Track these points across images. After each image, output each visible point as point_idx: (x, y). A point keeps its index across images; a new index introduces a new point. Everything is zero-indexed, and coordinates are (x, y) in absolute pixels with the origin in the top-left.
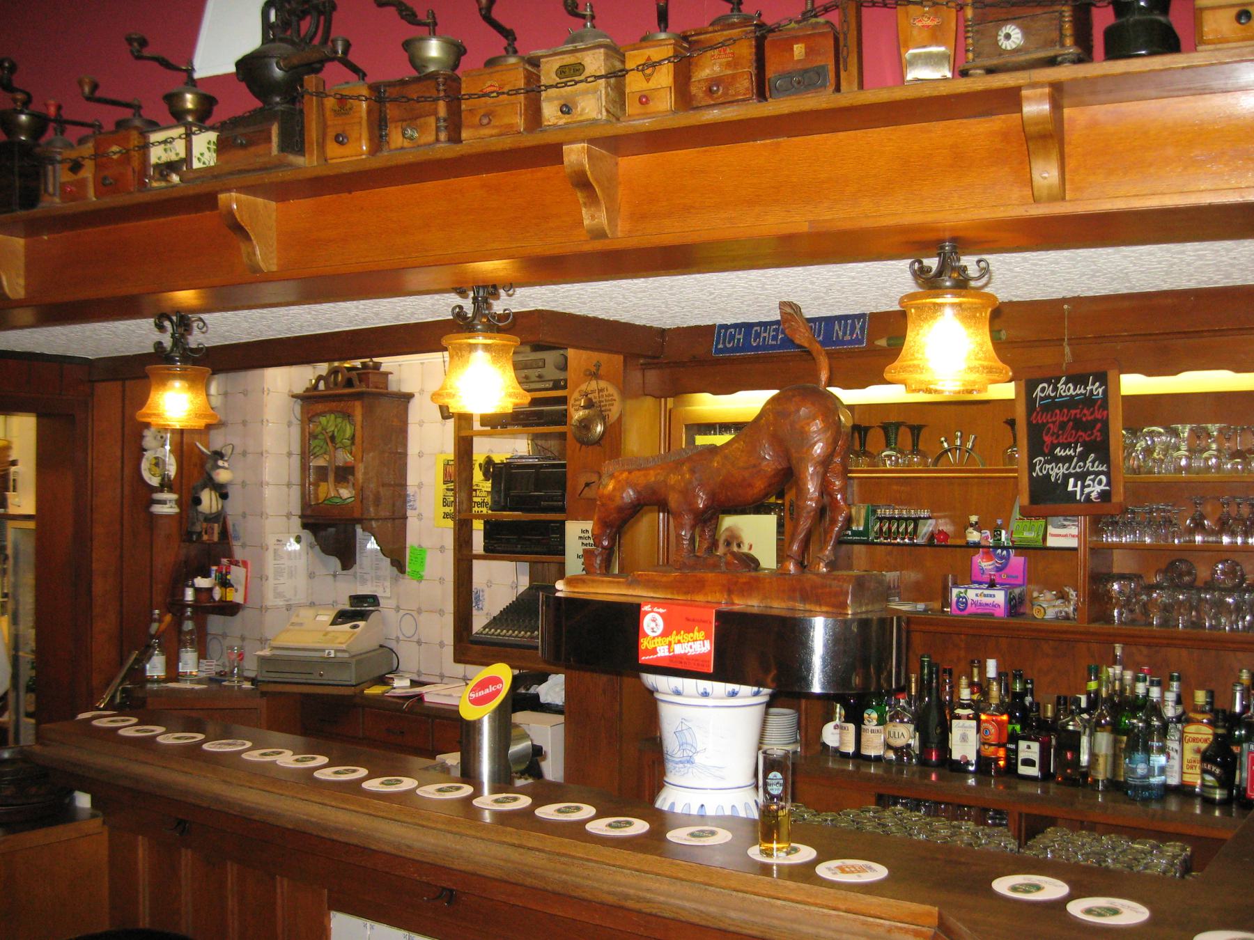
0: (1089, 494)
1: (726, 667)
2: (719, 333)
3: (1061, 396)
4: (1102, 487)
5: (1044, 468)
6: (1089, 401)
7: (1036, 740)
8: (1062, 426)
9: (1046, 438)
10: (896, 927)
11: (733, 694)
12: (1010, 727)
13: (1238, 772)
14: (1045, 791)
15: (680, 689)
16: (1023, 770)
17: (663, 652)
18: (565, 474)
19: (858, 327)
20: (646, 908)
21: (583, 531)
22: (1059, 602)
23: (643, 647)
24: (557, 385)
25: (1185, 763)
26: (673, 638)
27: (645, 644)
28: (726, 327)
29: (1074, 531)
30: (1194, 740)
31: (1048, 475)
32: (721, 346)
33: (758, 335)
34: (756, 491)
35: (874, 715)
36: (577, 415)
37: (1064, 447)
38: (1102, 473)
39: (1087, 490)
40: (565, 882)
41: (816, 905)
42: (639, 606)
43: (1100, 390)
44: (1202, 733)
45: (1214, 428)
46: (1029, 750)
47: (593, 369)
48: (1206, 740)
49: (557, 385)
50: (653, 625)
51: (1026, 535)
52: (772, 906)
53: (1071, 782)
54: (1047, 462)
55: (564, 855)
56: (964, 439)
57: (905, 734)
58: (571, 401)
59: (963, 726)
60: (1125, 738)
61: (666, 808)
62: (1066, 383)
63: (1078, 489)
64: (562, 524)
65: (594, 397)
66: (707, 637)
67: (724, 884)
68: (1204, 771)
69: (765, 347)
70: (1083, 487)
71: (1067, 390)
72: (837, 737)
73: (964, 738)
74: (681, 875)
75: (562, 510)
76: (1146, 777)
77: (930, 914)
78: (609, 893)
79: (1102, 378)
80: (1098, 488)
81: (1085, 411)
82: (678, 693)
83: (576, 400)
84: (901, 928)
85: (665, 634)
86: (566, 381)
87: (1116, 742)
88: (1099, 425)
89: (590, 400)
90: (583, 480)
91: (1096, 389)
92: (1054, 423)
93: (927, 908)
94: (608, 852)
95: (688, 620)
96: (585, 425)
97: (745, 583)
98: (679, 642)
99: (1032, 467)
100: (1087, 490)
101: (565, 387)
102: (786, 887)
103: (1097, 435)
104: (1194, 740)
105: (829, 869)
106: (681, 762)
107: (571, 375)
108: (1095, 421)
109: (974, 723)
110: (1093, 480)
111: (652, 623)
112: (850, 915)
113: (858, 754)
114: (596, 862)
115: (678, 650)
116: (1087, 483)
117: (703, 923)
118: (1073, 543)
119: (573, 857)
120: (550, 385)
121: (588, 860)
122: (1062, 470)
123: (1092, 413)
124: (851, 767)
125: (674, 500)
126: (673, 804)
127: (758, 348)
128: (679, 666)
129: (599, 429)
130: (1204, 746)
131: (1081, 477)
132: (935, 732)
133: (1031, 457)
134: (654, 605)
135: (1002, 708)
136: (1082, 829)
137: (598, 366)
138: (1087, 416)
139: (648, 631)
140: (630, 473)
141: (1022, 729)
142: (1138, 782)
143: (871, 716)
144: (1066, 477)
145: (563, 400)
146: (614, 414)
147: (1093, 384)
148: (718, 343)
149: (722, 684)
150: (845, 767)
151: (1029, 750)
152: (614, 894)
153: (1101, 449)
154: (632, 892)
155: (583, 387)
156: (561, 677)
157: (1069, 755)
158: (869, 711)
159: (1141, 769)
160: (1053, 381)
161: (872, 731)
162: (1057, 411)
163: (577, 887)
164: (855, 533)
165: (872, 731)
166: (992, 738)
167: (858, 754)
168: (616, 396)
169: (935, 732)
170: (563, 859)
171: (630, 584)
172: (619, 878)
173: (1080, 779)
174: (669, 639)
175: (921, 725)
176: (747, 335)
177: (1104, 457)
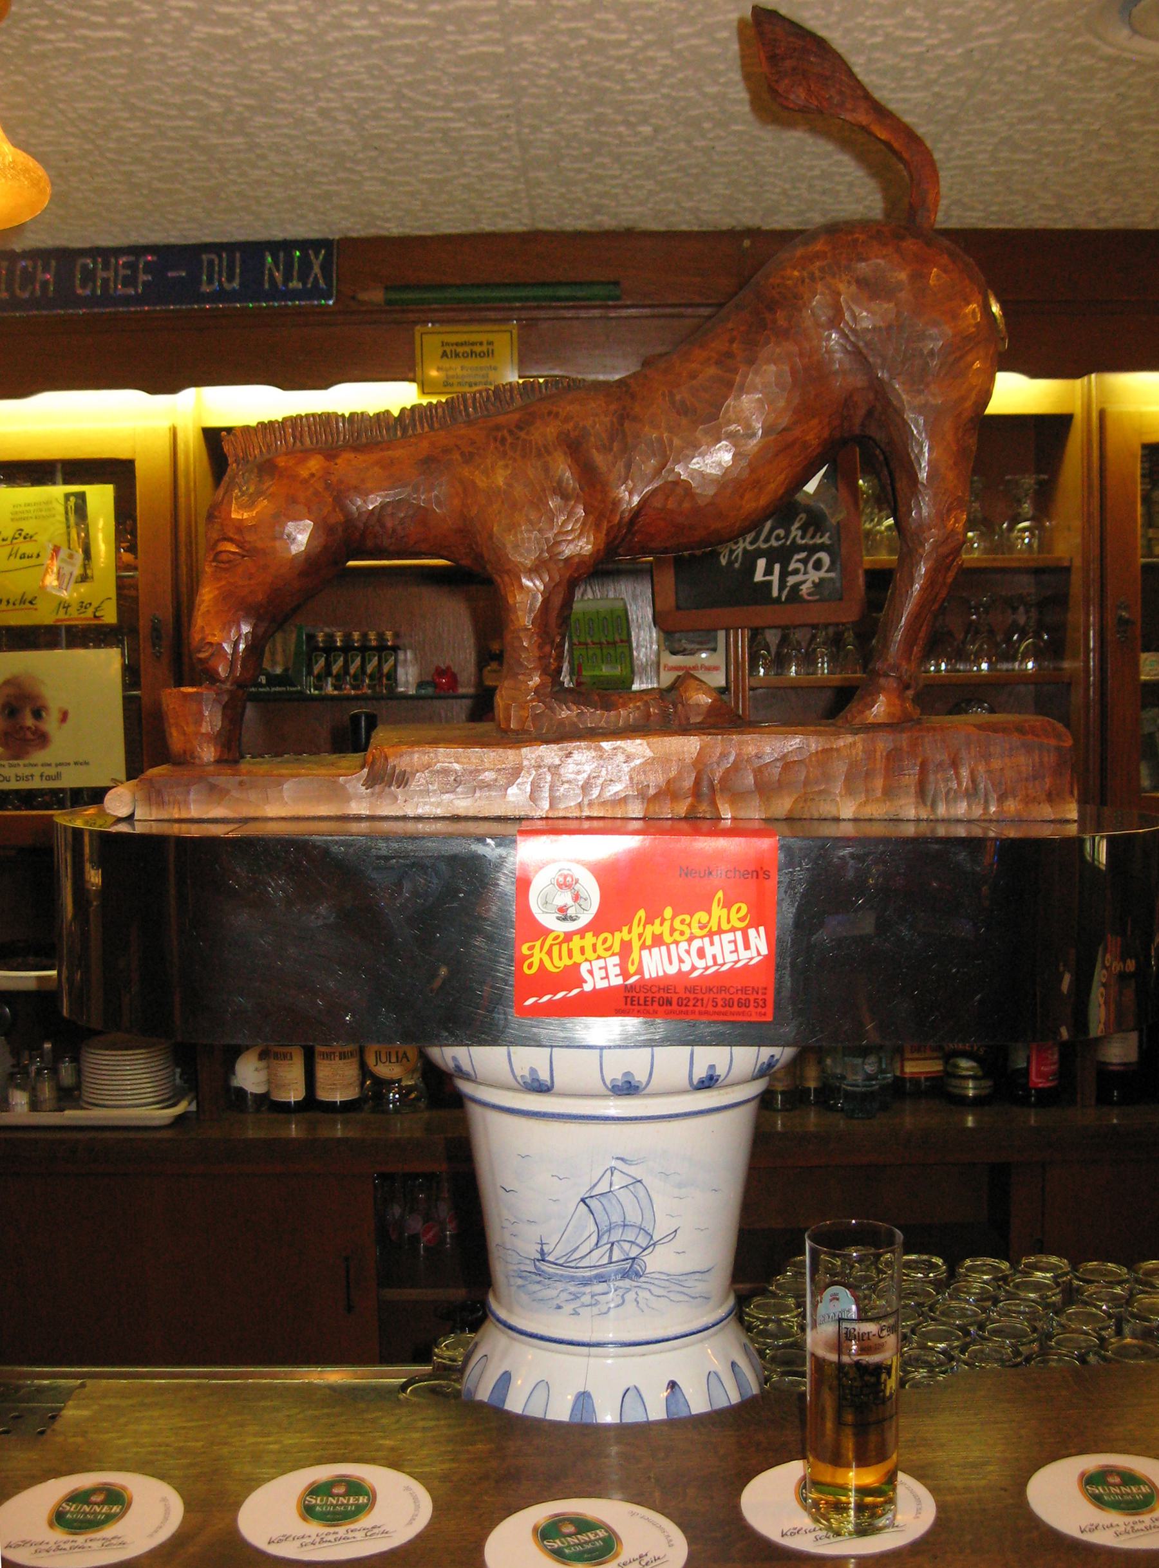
0: (796, 587)
4: (822, 574)
19: (317, 269)
26: (636, 931)
33: (89, 276)
38: (822, 548)
39: (792, 580)
63: (775, 578)
69: (107, 299)
72: (262, 1076)
80: (814, 576)
82: (541, 1088)
98: (658, 941)
100: (792, 580)
110: (805, 562)
113: (310, 1103)
116: (792, 566)
127: (93, 301)
131: (780, 556)
139: (548, 920)
150: (282, 1134)
164: (273, 680)
167: (310, 1103)
174: (624, 934)
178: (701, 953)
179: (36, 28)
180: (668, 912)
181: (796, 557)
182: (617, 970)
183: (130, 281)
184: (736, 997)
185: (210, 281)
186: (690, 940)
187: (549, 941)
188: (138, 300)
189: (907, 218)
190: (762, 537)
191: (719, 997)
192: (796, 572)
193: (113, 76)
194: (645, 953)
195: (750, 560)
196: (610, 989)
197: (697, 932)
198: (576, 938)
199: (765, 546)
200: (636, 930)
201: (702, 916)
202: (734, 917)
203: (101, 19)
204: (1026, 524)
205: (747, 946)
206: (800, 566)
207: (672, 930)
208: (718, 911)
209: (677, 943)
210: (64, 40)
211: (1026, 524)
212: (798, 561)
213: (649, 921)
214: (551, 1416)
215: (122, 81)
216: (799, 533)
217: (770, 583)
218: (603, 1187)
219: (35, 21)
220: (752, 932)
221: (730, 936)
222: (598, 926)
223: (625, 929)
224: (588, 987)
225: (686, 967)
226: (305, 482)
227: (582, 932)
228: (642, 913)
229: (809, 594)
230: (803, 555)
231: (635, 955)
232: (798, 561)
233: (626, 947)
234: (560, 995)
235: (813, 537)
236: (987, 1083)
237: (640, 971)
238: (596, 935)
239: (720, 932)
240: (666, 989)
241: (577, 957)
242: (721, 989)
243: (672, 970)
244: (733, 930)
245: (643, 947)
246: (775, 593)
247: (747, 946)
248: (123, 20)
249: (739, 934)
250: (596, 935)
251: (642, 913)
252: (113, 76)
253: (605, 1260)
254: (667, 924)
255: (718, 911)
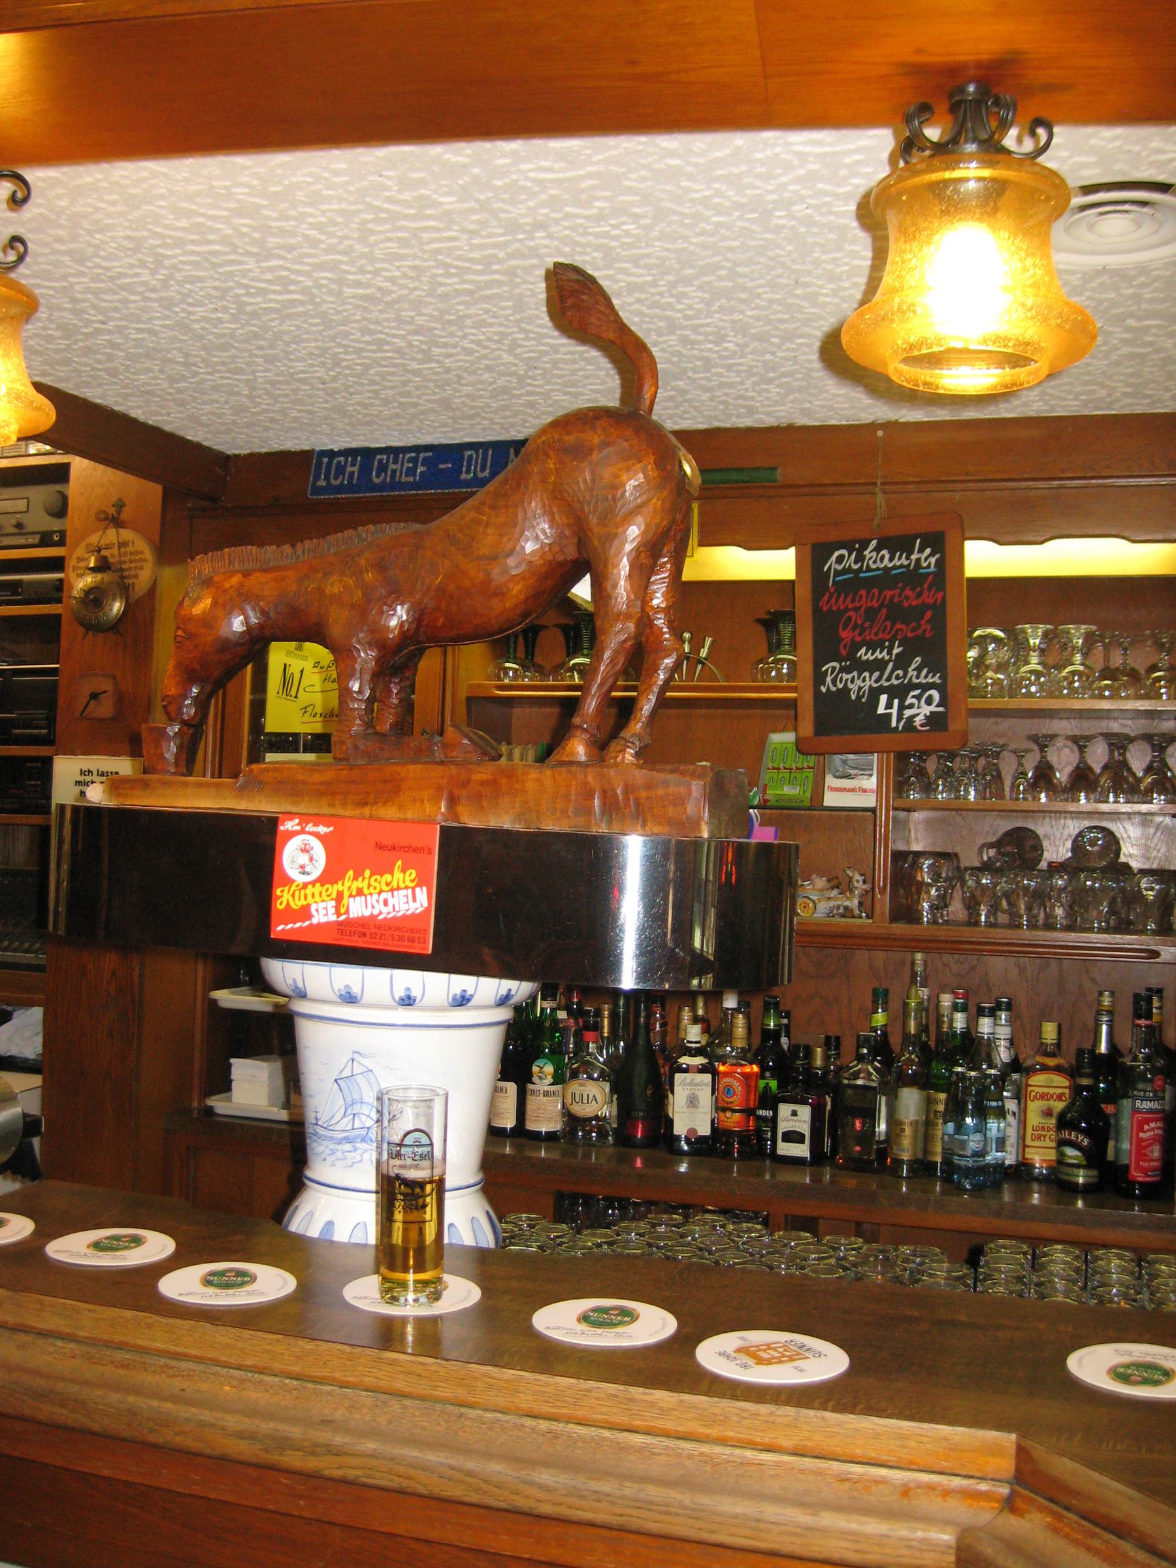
0: (911, 719)
1: (460, 939)
2: (320, 463)
3: (869, 569)
4: (933, 708)
5: (836, 678)
6: (913, 576)
7: (803, 1102)
8: (871, 614)
9: (844, 634)
10: (920, 1486)
11: (462, 1001)
12: (762, 1083)
13: (1111, 1143)
14: (816, 1179)
15: (356, 990)
16: (785, 1149)
17: (323, 913)
18: (54, 686)
20: (328, 1466)
21: (82, 773)
22: (834, 893)
23: (280, 906)
24: (46, 540)
25: (1029, 1131)
26: (348, 884)
27: (284, 898)
28: (331, 454)
29: (872, 783)
30: (1043, 1097)
31: (846, 690)
32: (322, 483)
33: (383, 468)
34: (509, 604)
35: (549, 1069)
36: (82, 583)
37: (872, 647)
39: (907, 713)
40: (132, 1412)
41: (723, 1441)
42: (272, 823)
43: (933, 560)
44: (1050, 1089)
45: (1077, 634)
46: (795, 1117)
47: (112, 511)
48: (1060, 1097)
49: (46, 540)
50: (303, 859)
51: (788, 790)
52: (624, 1448)
53: (858, 1166)
54: (843, 670)
55: (122, 1346)
56: (697, 645)
57: (595, 1099)
58: (71, 563)
59: (692, 1083)
60: (942, 1096)
61: (314, 1232)
62: (877, 549)
63: (894, 711)
64: (48, 762)
65: (112, 554)
66: (421, 882)
67: (501, 1401)
68: (1062, 1143)
69: (394, 485)
70: (902, 708)
71: (877, 560)
73: (693, 1102)
74: (400, 1385)
75: (48, 741)
76: (982, 1153)
77: (995, 1450)
78: (240, 1435)
79: (935, 541)
80: (926, 710)
81: (908, 592)
82: (350, 999)
83: (80, 560)
84: (930, 1487)
85: (330, 876)
86: (63, 534)
87: (929, 1102)
88: (929, 614)
89: (105, 558)
90: (86, 690)
91: (927, 559)
92: (856, 609)
93: (991, 1435)
94: (225, 1336)
95: (380, 847)
96: (95, 598)
97: (483, 783)
98: (360, 892)
99: (819, 678)
100: (907, 713)
101: (61, 543)
102: (652, 1404)
103: (925, 627)
104: (1043, 1097)
105: (723, 1354)
106: (347, 1140)
107: (72, 522)
108: (925, 607)
109: (707, 1078)
110: (918, 697)
111: (301, 855)
112: (808, 1462)
114: (199, 1360)
115: (357, 909)
117: (474, 1498)
118: (870, 801)
119: (144, 1350)
120: (36, 539)
121: (177, 1356)
122: (868, 681)
123: (919, 595)
124: (508, 1150)
125: (337, 621)
126: (330, 1225)
127: (381, 487)
128: (360, 943)
129: (117, 607)
130: (1059, 1106)
131: (899, 692)
132: (641, 1091)
133: (818, 663)
134: (305, 818)
135: (745, 1055)
136: (858, 1235)
137: (120, 505)
138: (910, 598)
139: (292, 872)
140: (246, 575)
141: (779, 1087)
142: (970, 1163)
143: (544, 1069)
144: (875, 693)
145: (57, 564)
146: (143, 578)
147: (921, 551)
148: (317, 478)
149: (444, 977)
151: (795, 1117)
152: (252, 1437)
153: (931, 648)
154: (296, 1432)
155: (94, 539)
156: (37, 1013)
157: (858, 1124)
158: (540, 1062)
159: (974, 1142)
160: (857, 546)
161: (546, 1094)
162: (863, 592)
163: (167, 1422)
165: (546, 1094)
166: (736, 1101)
168: (148, 554)
169: (641, 1091)
170: (120, 1355)
171: (242, 791)
172: (253, 1395)
173: (878, 1160)
174: (338, 886)
175: (619, 1081)
176: (365, 469)
177: (936, 660)
178: (386, 903)
179: (437, 275)
180: (367, 873)
181: (912, 693)
182: (333, 910)
183: (411, 472)
184: (406, 935)
185: (468, 472)
186: (379, 894)
187: (293, 888)
188: (415, 486)
189: (630, 418)
190: (885, 677)
191: (396, 933)
192: (911, 706)
193: (504, 309)
194: (351, 899)
195: (875, 693)
196: (328, 923)
197: (385, 888)
198: (310, 886)
199: (886, 684)
200: (347, 883)
201: (387, 877)
202: (407, 879)
203: (480, 267)
204: (1161, 673)
205: (414, 900)
206: (914, 701)
207: (369, 886)
208: (398, 874)
209: (371, 894)
210: (459, 283)
211: (1161, 673)
212: (913, 697)
213: (355, 878)
214: (309, 1234)
215: (510, 312)
216: (915, 673)
217: (890, 714)
218: (347, 1073)
219: (435, 271)
220: (418, 890)
221: (404, 892)
222: (324, 879)
223: (340, 883)
224: (315, 921)
225: (376, 912)
226: (226, 590)
227: (313, 883)
228: (351, 873)
229: (922, 725)
230: (917, 692)
231: (345, 902)
232: (913, 697)
233: (340, 896)
234: (290, 926)
235: (926, 677)
236: (1094, 1173)
237: (347, 912)
238: (322, 885)
239: (398, 889)
240: (363, 926)
241: (310, 900)
242: (397, 929)
243: (367, 913)
244: (407, 888)
245: (351, 896)
246: (894, 724)
247: (414, 900)
248: (496, 267)
249: (410, 891)
250: (322, 885)
251: (351, 873)
252: (504, 309)
253: (350, 1127)
254: (366, 881)
255: (398, 874)
